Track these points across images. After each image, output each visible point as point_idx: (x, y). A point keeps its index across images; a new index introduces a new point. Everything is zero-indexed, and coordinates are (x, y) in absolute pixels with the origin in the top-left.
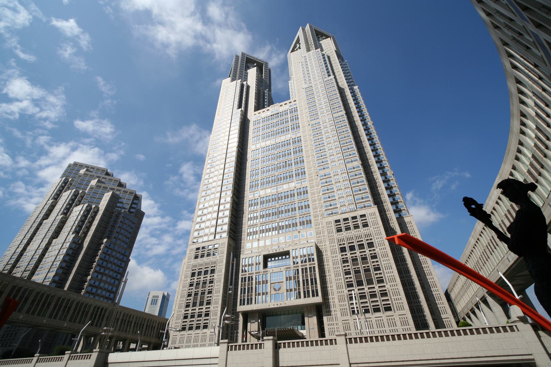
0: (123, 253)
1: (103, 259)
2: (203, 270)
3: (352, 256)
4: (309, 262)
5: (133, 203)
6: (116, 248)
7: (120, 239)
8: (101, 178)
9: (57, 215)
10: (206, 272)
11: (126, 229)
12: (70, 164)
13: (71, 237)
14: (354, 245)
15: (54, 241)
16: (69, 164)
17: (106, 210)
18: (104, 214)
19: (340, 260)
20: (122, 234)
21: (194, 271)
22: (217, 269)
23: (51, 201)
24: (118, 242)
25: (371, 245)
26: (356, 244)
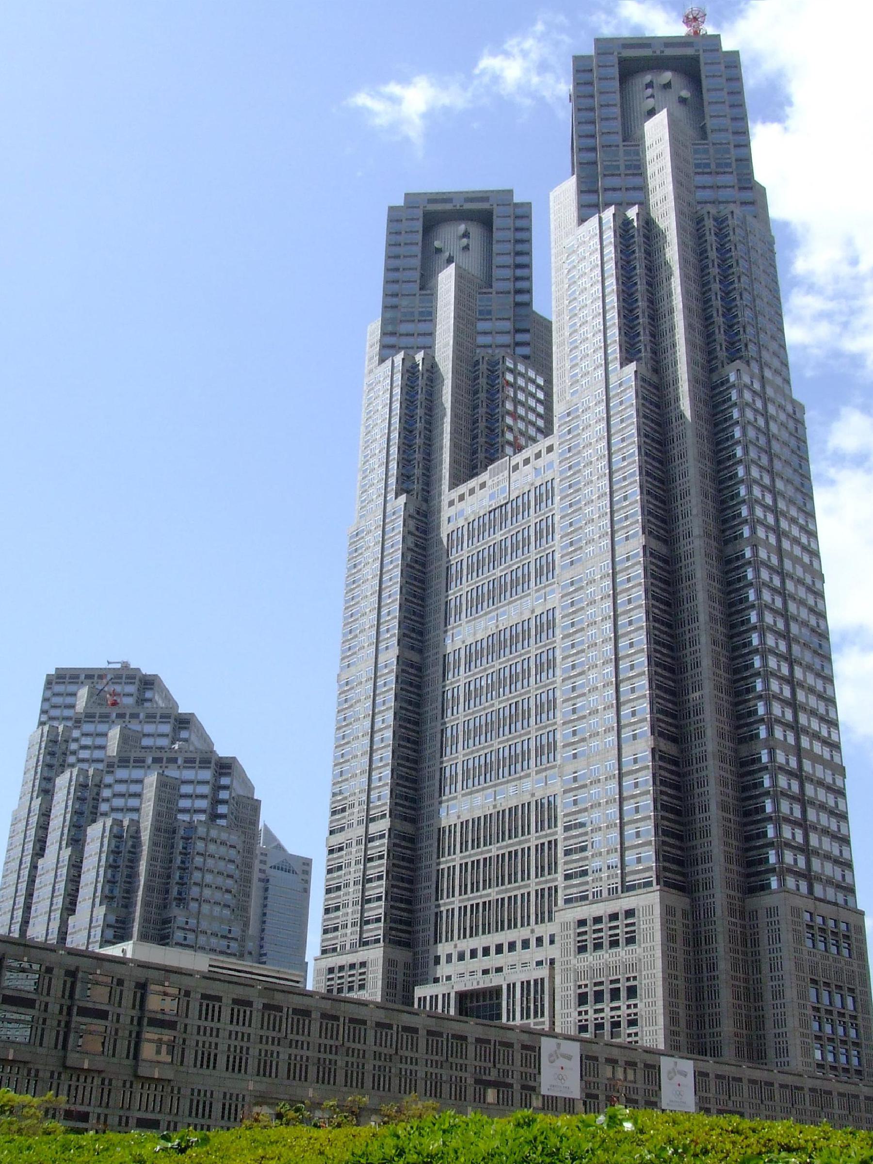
0: (226, 933)
1: (184, 929)
2: (606, 988)
3: (596, 1016)
4: (534, 1018)
5: (218, 788)
6: (204, 925)
7: (207, 901)
8: (128, 716)
9: (32, 799)
10: (615, 994)
11: (216, 871)
12: (48, 675)
13: (100, 911)
14: (619, 988)
15: (71, 920)
16: (45, 677)
17: (157, 829)
18: (154, 843)
19: (575, 1023)
20: (208, 886)
21: (583, 990)
22: (642, 985)
23: (37, 803)
24: (205, 908)
25: (632, 992)
26: (623, 986)
